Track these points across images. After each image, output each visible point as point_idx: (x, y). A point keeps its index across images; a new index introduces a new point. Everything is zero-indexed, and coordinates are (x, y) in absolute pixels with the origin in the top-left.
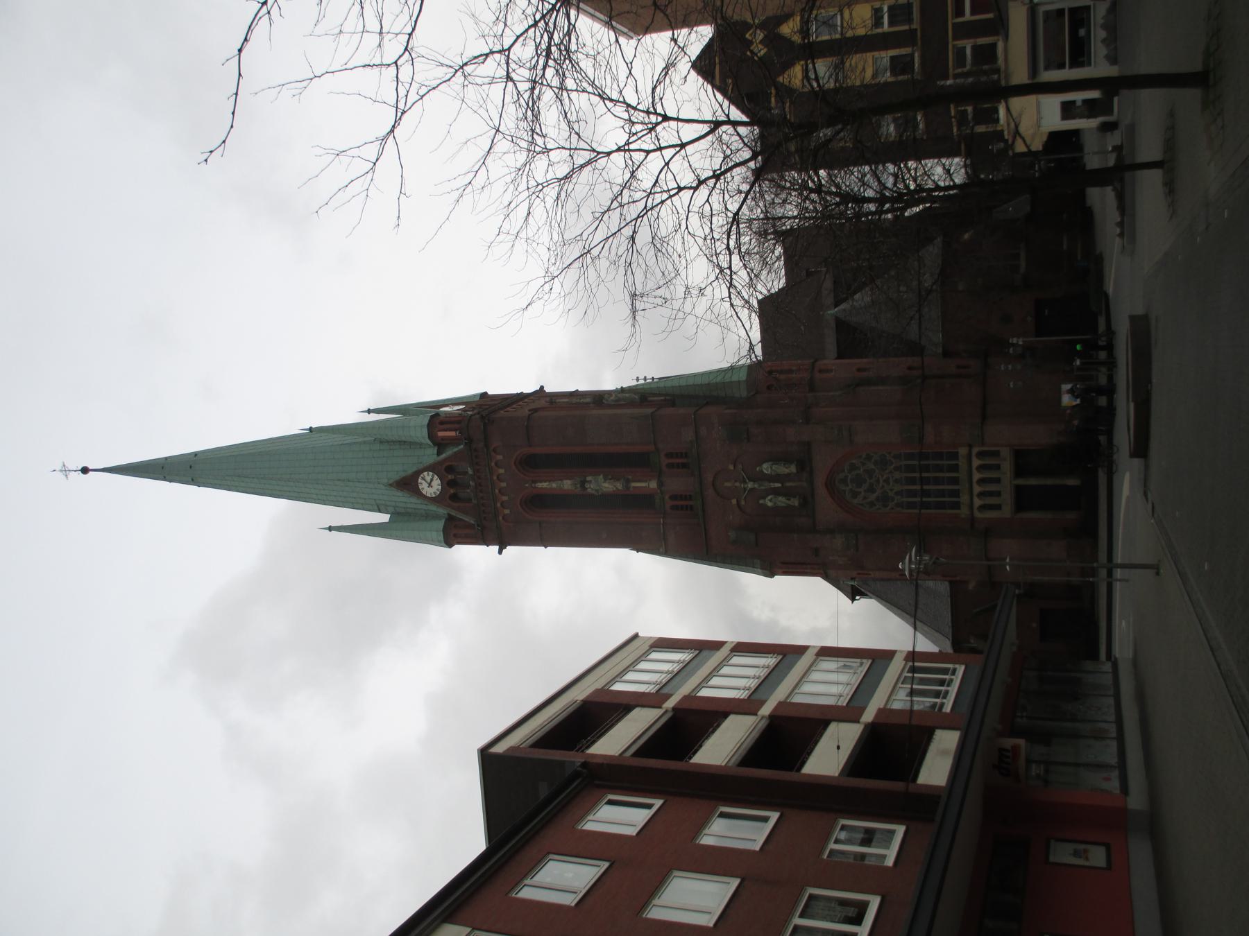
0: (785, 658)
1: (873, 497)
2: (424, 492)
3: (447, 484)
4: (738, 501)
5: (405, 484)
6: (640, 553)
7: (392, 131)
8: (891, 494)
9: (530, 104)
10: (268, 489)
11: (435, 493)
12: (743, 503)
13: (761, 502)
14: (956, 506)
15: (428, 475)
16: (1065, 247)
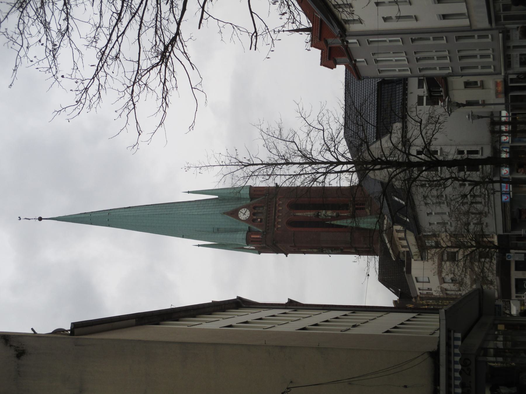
2: (240, 218)
3: (253, 214)
5: (231, 214)
6: (290, 255)
10: (470, 236)
11: (246, 218)
15: (244, 210)
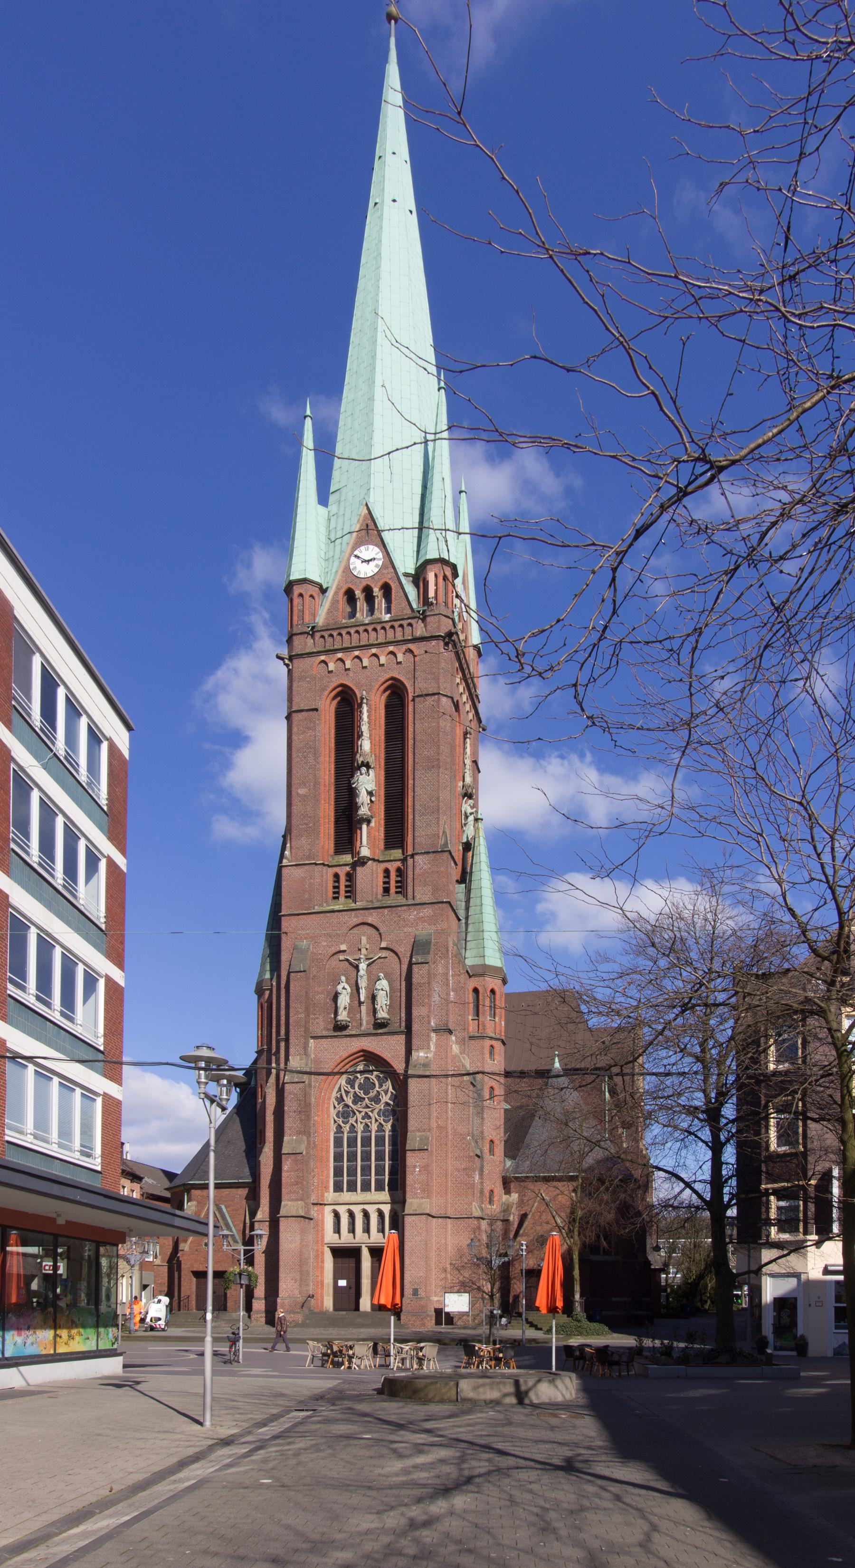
0: (561, 1473)
1: (349, 1101)
4: (344, 951)
7: (817, 149)
8: (352, 1121)
9: (814, 649)
11: (355, 568)
12: (342, 957)
13: (343, 978)
14: (338, 1188)
16: (614, 1299)
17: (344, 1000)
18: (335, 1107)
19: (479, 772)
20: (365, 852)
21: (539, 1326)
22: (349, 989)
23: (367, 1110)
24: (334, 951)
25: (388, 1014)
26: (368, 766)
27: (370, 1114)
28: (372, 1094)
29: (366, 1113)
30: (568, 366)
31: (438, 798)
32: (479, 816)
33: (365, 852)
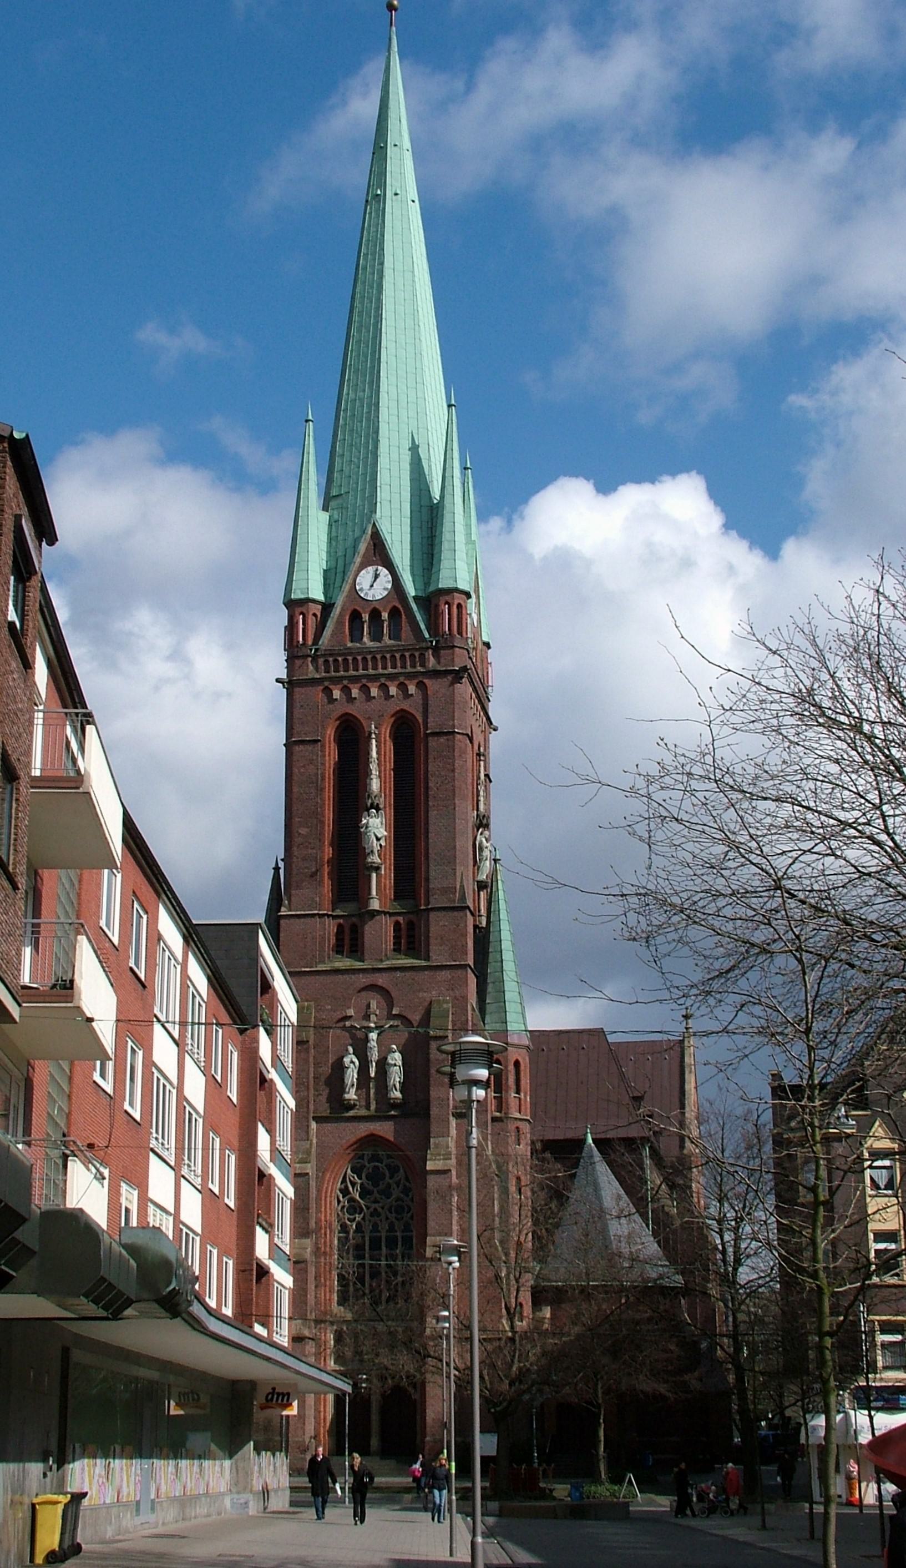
17: (352, 1075)
18: (339, 1202)
19: (491, 781)
20: (375, 905)
21: (281, 947)
22: (357, 1063)
23: (376, 1205)
24: (340, 1017)
25: (401, 1092)
26: (378, 809)
27: (379, 1210)
28: (382, 1186)
29: (375, 1209)
30: (615, 1034)
31: (455, 847)
32: (498, 857)
33: (375, 905)
